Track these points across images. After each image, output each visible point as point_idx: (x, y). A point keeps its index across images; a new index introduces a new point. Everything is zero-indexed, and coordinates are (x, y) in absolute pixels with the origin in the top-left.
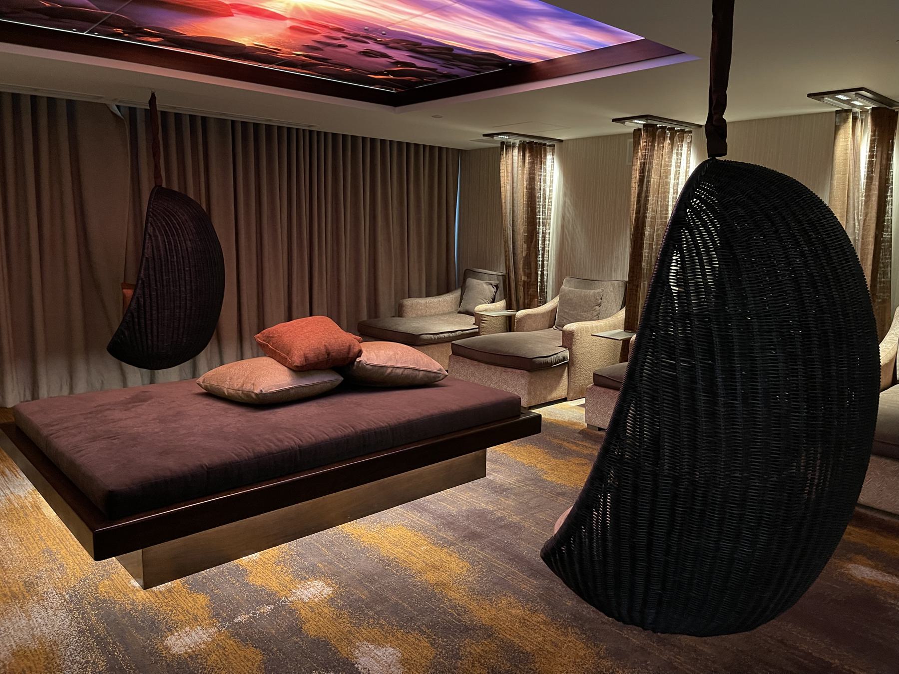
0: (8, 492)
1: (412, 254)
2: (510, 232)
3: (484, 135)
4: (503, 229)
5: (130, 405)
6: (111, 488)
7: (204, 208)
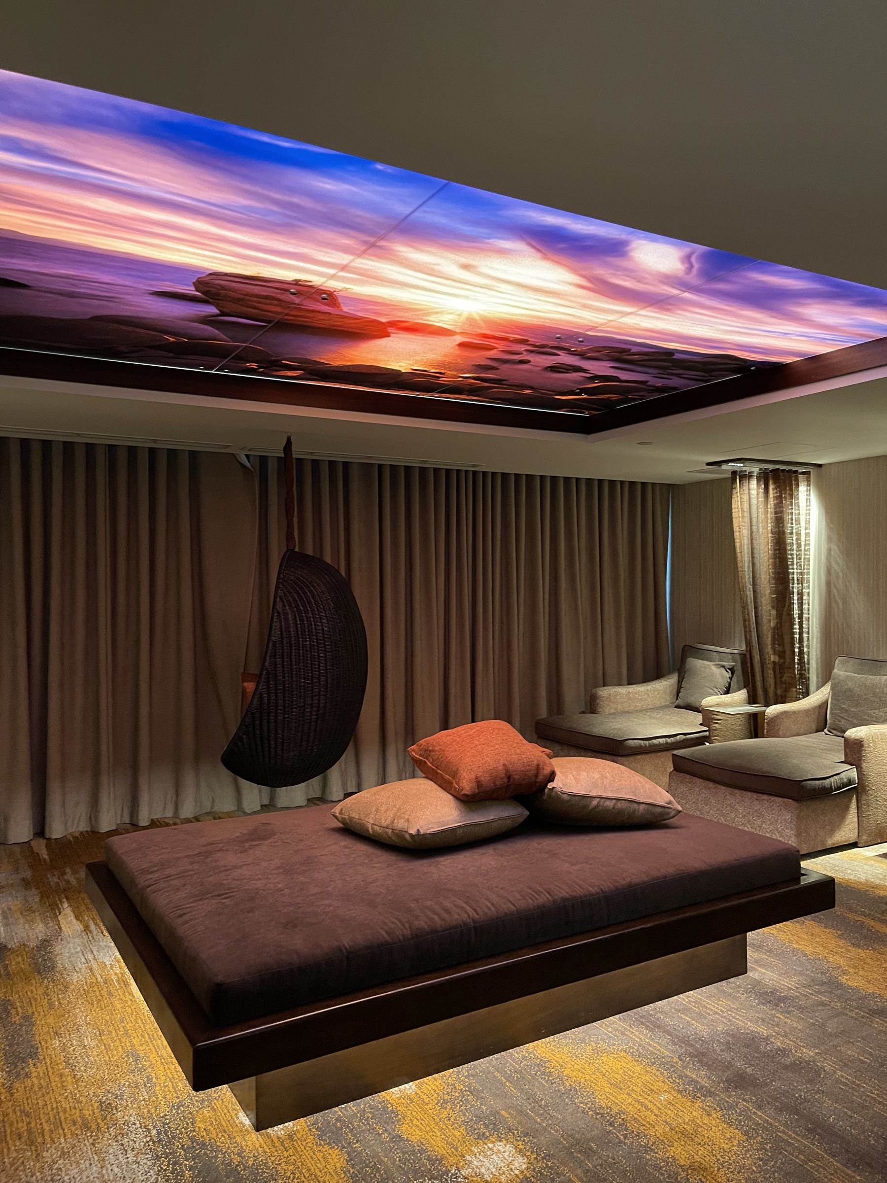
0: (90, 957)
1: (606, 626)
2: (750, 594)
3: (708, 464)
4: (742, 590)
5: (247, 845)
6: (220, 979)
7: (343, 574)
